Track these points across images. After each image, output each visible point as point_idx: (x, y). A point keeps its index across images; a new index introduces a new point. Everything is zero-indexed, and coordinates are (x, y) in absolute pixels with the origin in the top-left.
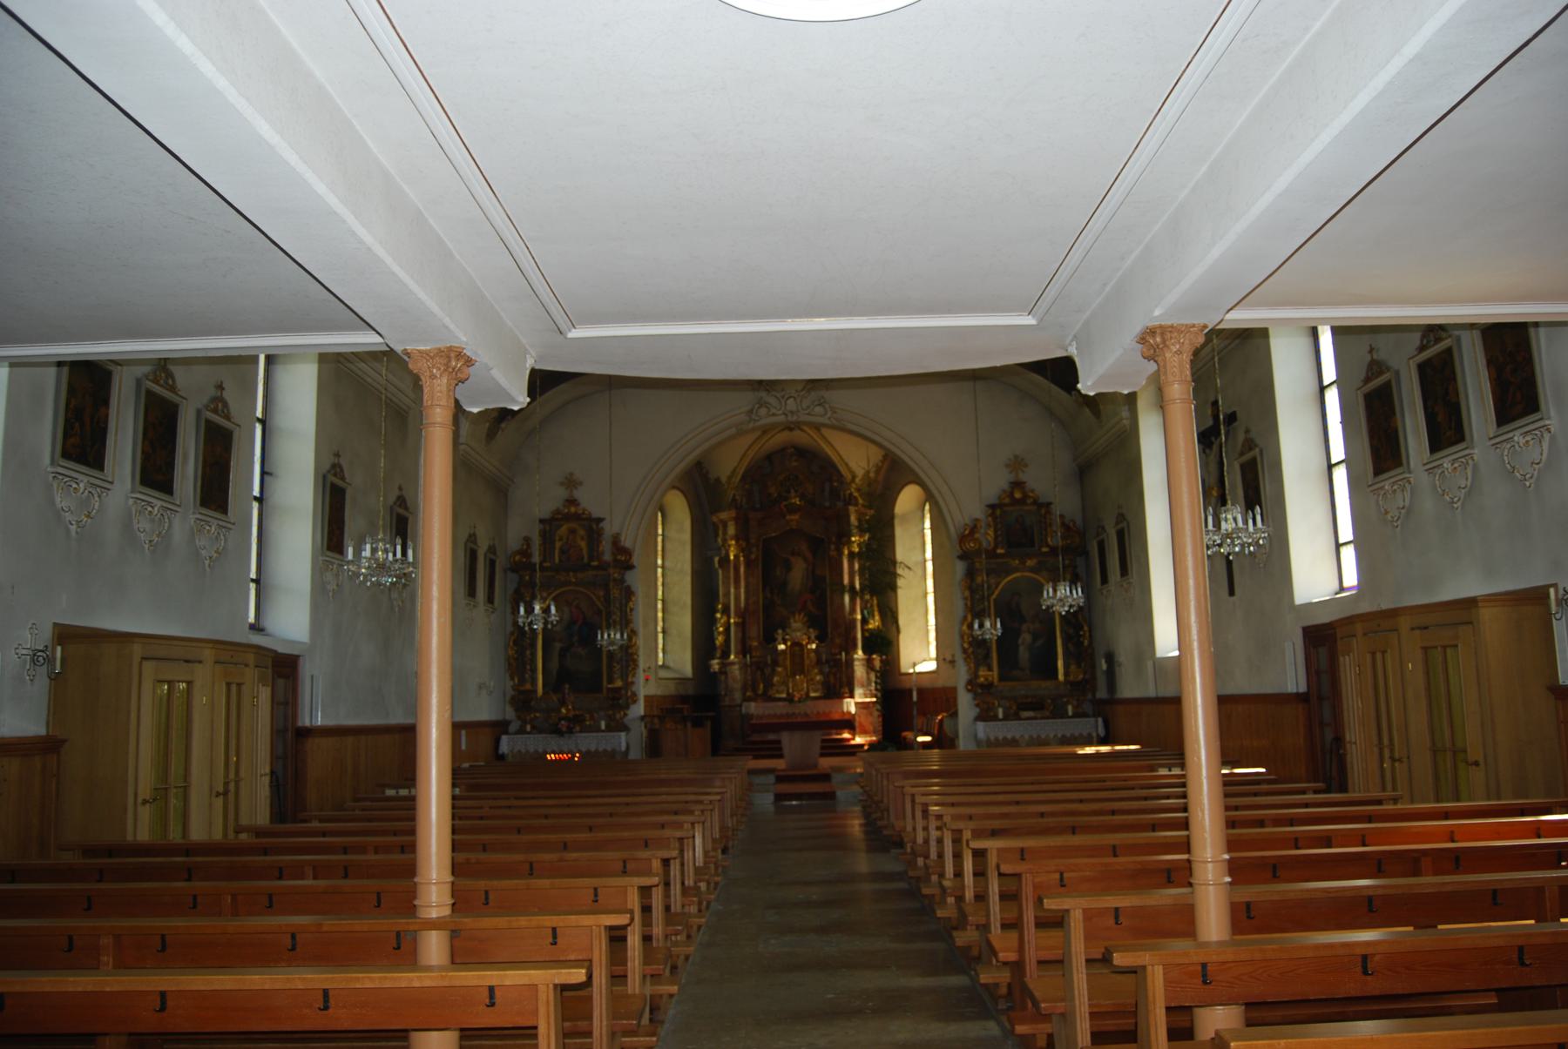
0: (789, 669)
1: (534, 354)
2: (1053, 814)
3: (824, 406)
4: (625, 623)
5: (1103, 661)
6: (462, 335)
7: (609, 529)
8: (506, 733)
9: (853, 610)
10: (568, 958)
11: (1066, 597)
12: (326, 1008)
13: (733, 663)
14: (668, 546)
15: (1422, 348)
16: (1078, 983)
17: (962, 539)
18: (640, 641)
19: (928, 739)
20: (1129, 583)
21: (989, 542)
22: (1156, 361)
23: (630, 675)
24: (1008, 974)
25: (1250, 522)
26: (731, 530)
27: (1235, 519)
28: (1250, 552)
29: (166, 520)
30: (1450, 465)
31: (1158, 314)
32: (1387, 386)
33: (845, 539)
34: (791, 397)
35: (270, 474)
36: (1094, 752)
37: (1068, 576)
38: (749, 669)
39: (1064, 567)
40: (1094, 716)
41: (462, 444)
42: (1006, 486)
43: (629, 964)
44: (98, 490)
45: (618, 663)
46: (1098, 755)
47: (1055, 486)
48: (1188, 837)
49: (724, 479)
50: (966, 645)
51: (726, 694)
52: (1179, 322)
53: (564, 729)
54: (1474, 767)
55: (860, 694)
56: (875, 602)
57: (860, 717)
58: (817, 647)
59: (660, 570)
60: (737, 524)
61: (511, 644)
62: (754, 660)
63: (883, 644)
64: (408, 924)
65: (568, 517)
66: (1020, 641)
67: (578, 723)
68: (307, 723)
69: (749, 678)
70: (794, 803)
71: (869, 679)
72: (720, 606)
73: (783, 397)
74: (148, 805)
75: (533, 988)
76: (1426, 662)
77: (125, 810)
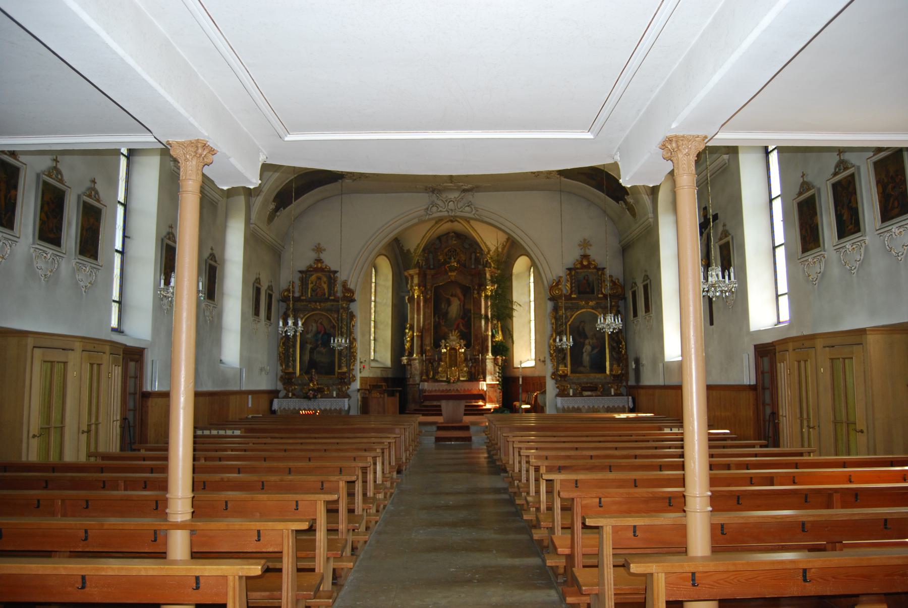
0: (448, 363)
1: (265, 153)
2: (598, 457)
3: (471, 207)
4: (349, 334)
5: (633, 363)
6: (205, 131)
7: (342, 277)
8: (278, 397)
9: (487, 330)
10: (268, 550)
11: (612, 323)
13: (415, 359)
14: (378, 289)
15: (835, 174)
16: (608, 576)
17: (551, 288)
18: (358, 345)
19: (528, 406)
20: (651, 317)
21: (567, 290)
22: (671, 161)
23: (352, 365)
24: (564, 561)
25: (727, 277)
26: (416, 281)
27: (717, 275)
28: (726, 296)
29: (56, 262)
30: (850, 246)
31: (675, 127)
32: (812, 198)
33: (482, 288)
34: (452, 201)
35: (129, 238)
36: (625, 417)
37: (614, 312)
39: (610, 306)
40: (627, 395)
41: (252, 224)
42: (578, 257)
43: (317, 551)
45: (344, 358)
46: (628, 419)
47: (607, 256)
48: (683, 462)
49: (412, 251)
50: (552, 352)
51: (410, 377)
52: (688, 134)
53: (311, 396)
54: (860, 433)
55: (490, 379)
56: (499, 325)
57: (488, 392)
59: (373, 304)
60: (419, 277)
61: (281, 344)
62: (427, 357)
63: (503, 350)
64: (160, 525)
65: (316, 270)
66: (584, 350)
67: (319, 392)
68: (149, 389)
69: (424, 368)
71: (495, 370)
72: (408, 325)
73: (446, 201)
74: (36, 438)
75: (225, 577)
76: (832, 367)
77: (21, 442)
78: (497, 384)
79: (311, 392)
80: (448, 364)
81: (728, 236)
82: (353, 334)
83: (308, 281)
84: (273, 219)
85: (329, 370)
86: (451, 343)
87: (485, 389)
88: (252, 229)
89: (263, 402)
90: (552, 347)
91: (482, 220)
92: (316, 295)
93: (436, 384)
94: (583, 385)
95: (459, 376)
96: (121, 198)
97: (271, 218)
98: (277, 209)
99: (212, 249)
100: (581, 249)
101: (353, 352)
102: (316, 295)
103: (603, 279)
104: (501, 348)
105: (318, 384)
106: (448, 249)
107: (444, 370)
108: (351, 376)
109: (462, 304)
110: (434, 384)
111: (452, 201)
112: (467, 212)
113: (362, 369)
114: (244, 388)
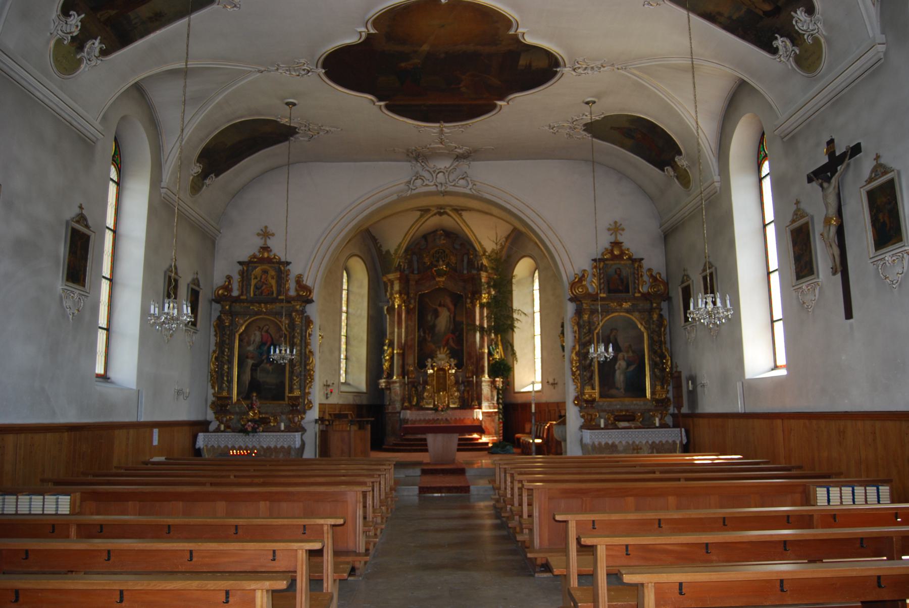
0: (435, 386)
3: (467, 180)
7: (295, 270)
8: (207, 431)
9: (482, 346)
12: (191, 560)
13: (395, 382)
14: (351, 298)
17: (573, 285)
26: (397, 287)
29: (82, 301)
32: (891, 182)
33: (477, 296)
34: (441, 172)
38: (407, 386)
42: (608, 246)
44: (83, 297)
45: (297, 377)
49: (392, 252)
51: (389, 405)
53: (250, 429)
55: (486, 406)
57: (485, 422)
58: (455, 372)
59: (344, 316)
60: (400, 282)
61: (213, 359)
62: (410, 380)
65: (262, 261)
66: (617, 366)
67: (262, 424)
69: (407, 393)
70: (436, 495)
72: (387, 341)
73: (434, 172)
78: (495, 412)
79: (250, 423)
80: (435, 388)
81: (689, 281)
82: (310, 345)
83: (251, 275)
84: (200, 188)
85: (277, 394)
86: (439, 362)
87: (481, 419)
88: (163, 194)
89: (181, 439)
90: (574, 362)
91: (481, 197)
92: (262, 293)
93: (421, 412)
94: (616, 414)
95: (449, 403)
96: (110, 224)
97: (197, 186)
98: (204, 175)
99: (81, 207)
100: (611, 234)
101: (309, 370)
102: (262, 293)
103: (640, 273)
104: (502, 367)
105: (259, 412)
106: (436, 249)
107: (430, 395)
108: (306, 402)
109: (452, 316)
110: (417, 412)
111: (441, 172)
112: (462, 187)
113: (329, 393)
114: (143, 419)
